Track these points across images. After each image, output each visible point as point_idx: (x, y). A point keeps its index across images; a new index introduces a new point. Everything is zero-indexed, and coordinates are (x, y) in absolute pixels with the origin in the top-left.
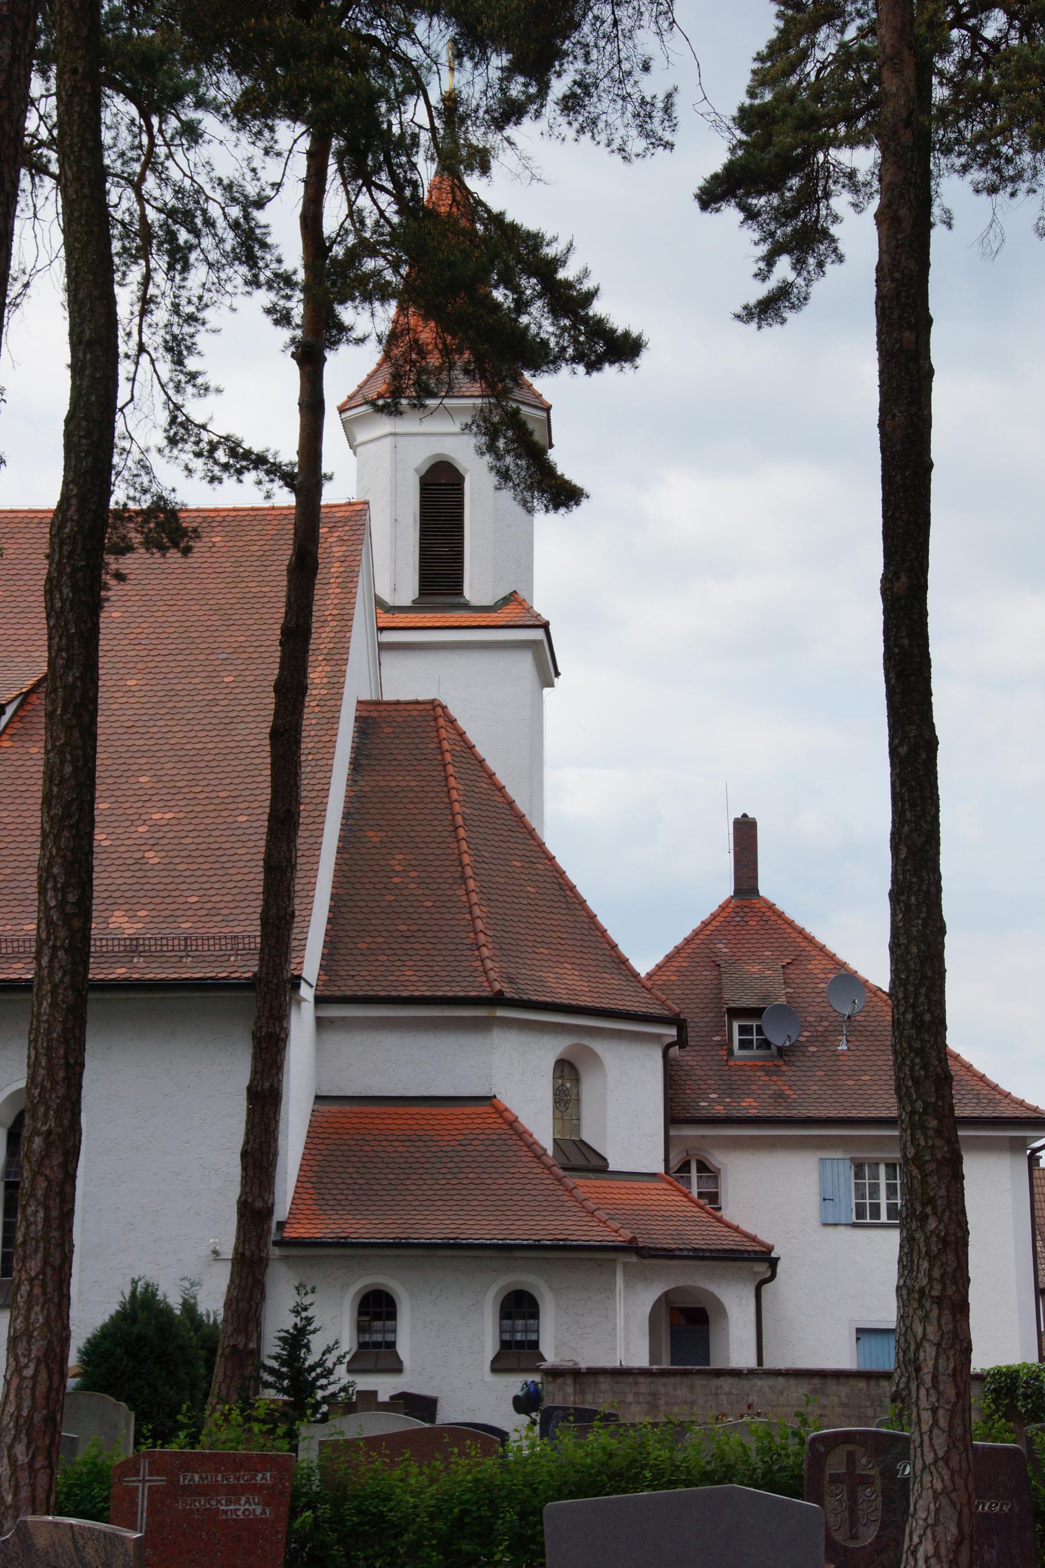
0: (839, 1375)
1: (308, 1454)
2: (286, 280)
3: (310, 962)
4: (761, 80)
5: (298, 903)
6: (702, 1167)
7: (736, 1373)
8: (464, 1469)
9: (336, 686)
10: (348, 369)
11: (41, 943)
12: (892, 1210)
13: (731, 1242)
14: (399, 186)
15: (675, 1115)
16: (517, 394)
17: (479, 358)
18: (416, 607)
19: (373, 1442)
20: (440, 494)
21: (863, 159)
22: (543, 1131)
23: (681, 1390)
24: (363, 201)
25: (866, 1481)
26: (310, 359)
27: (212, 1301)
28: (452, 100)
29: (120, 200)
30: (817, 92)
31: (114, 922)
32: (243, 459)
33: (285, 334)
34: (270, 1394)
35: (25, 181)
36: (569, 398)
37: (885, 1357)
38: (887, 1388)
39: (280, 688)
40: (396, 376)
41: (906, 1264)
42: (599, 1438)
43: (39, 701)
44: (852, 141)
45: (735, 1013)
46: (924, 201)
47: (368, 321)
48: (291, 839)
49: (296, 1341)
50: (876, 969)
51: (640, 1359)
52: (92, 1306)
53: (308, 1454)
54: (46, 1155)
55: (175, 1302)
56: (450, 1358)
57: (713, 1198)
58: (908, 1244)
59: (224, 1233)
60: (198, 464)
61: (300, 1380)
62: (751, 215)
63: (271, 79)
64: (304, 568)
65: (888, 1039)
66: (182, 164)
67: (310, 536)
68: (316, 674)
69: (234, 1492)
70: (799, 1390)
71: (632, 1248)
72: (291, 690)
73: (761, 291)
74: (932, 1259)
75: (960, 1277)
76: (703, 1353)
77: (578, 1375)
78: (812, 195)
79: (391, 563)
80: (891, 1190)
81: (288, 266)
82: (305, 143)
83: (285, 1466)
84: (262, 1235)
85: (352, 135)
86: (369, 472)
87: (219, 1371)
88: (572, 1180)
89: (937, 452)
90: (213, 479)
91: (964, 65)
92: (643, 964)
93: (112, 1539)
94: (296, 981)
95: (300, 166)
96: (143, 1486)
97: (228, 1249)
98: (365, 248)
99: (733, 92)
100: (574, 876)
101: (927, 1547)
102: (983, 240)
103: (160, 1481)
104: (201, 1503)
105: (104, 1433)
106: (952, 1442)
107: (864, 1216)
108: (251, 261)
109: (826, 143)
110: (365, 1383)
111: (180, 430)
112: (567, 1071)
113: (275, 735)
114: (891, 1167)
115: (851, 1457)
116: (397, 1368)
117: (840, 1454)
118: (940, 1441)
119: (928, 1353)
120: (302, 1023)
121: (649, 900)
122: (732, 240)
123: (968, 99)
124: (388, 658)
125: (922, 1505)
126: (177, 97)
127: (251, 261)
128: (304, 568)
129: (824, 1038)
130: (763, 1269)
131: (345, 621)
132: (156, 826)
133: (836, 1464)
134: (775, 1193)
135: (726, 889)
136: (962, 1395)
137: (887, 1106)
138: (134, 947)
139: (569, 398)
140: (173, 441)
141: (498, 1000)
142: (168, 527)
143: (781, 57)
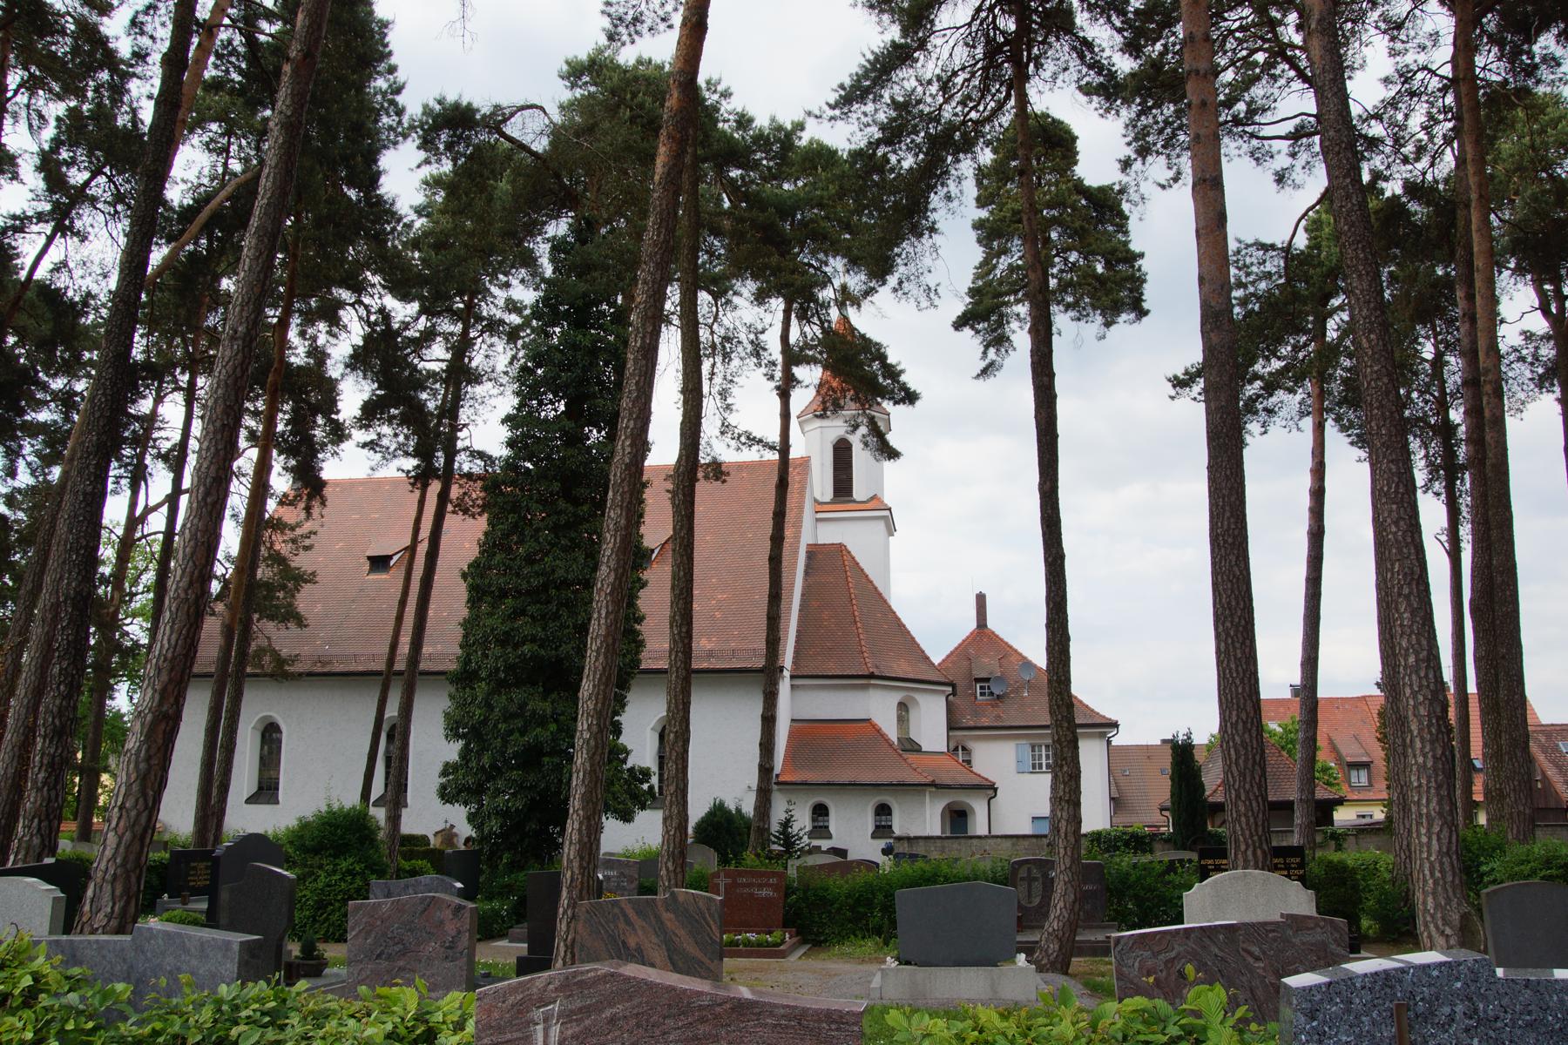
0: (1024, 837)
1: (792, 872)
2: (774, 364)
3: (787, 659)
4: (977, 277)
5: (782, 634)
6: (964, 749)
7: (979, 837)
8: (862, 878)
9: (797, 537)
10: (802, 398)
11: (671, 650)
12: (1048, 766)
13: (977, 781)
14: (822, 323)
15: (952, 726)
16: (875, 407)
17: (857, 394)
18: (832, 502)
19: (821, 866)
20: (842, 452)
21: (1022, 309)
22: (892, 733)
23: (955, 845)
24: (807, 329)
25: (1036, 879)
26: (784, 394)
27: (749, 808)
28: (844, 287)
29: (704, 334)
30: (1001, 282)
31: (701, 644)
32: (752, 440)
33: (772, 384)
34: (775, 847)
35: (664, 329)
36: (898, 417)
37: (1044, 829)
38: (1046, 841)
39: (772, 538)
40: (824, 402)
41: (1054, 788)
42: (920, 864)
43: (669, 547)
44: (1018, 301)
45: (978, 680)
46: (1049, 325)
47: (810, 375)
48: (779, 606)
49: (786, 824)
50: (1040, 659)
51: (938, 833)
52: (697, 810)
53: (792, 872)
54: (676, 742)
55: (733, 808)
56: (853, 832)
57: (969, 762)
58: (1055, 778)
59: (753, 779)
60: (733, 443)
61: (788, 840)
62: (978, 332)
63: (768, 282)
64: (782, 485)
65: (1046, 690)
66: (728, 319)
67: (785, 473)
68: (788, 533)
69: (760, 886)
70: (1008, 843)
71: (933, 784)
72: (777, 539)
73: (983, 364)
74: (1065, 784)
75: (1077, 791)
76: (965, 828)
77: (910, 840)
78: (1000, 324)
79: (821, 483)
80: (1047, 757)
81: (773, 358)
82: (782, 306)
83: (782, 876)
84: (769, 780)
85: (800, 295)
86: (811, 444)
87: (752, 837)
88: (906, 755)
89: (1060, 430)
90: (738, 449)
91: (1061, 271)
92: (936, 660)
93: (710, 899)
94: (781, 669)
95: (780, 316)
96: (722, 882)
97: (755, 787)
98: (806, 346)
99: (965, 280)
100: (904, 620)
101: (1061, 904)
102: (1074, 341)
103: (729, 881)
104: (746, 890)
105: (704, 860)
106: (1073, 861)
107: (1036, 768)
108: (758, 355)
109: (1007, 304)
110: (815, 843)
111: (725, 428)
112: (903, 706)
113: (771, 559)
114: (1047, 747)
115: (1029, 870)
116: (830, 837)
117: (1025, 868)
118: (1068, 861)
119: (1063, 824)
120: (784, 687)
121: (938, 631)
122: (970, 342)
123: (1064, 286)
124: (820, 525)
125: (1059, 888)
126: (726, 292)
127: (758, 355)
128: (782, 485)
129: (1017, 691)
130: (991, 792)
131: (801, 508)
132: (719, 601)
133: (1023, 873)
134: (997, 759)
135: (974, 625)
136: (1077, 841)
137: (1046, 719)
138: (710, 654)
139: (898, 417)
140: (722, 433)
141: (872, 676)
142: (718, 471)
143: (986, 266)
